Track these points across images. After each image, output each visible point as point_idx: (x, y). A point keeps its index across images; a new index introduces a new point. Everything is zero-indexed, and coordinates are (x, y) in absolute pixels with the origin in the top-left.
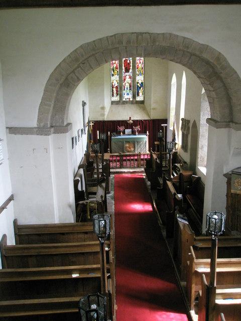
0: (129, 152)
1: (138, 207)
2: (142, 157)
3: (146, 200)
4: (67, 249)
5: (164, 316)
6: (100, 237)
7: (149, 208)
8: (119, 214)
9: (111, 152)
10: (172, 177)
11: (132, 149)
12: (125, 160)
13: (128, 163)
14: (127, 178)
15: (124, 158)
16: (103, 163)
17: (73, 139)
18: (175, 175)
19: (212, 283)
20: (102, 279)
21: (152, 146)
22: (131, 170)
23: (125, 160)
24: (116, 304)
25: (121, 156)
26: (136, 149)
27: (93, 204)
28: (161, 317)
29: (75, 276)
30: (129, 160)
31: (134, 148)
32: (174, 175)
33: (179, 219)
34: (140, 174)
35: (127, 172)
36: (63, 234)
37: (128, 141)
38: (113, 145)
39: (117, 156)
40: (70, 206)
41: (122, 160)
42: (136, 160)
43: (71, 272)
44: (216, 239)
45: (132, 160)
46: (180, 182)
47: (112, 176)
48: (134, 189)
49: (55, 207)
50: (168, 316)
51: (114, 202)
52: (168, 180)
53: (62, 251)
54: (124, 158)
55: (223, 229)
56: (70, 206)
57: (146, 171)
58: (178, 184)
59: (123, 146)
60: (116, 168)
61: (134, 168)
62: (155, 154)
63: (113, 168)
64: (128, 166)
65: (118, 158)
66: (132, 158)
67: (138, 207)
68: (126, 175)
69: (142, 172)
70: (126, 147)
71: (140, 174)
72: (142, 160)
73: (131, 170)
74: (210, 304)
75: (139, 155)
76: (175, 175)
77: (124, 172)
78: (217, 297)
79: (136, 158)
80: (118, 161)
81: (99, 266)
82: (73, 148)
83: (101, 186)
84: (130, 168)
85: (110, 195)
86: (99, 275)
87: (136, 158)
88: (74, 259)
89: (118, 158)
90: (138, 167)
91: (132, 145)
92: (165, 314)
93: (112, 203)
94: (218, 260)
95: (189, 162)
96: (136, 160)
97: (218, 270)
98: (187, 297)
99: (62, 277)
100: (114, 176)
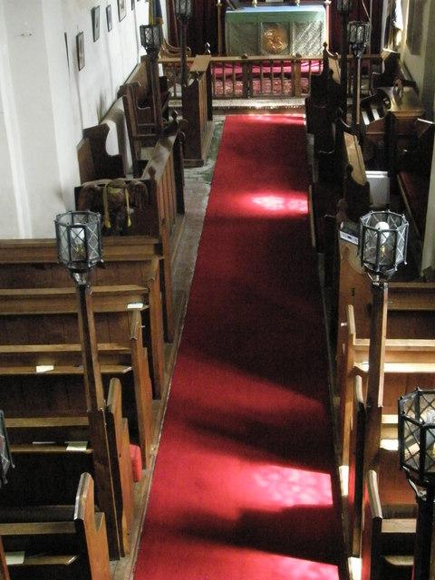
0: (273, 52)
1: (270, 203)
2: (305, 68)
3: (290, 185)
4: (41, 304)
5: (275, 477)
6: (76, 271)
7: (300, 205)
8: (215, 221)
9: (214, 53)
10: (367, 122)
11: (283, 46)
12: (257, 76)
13: (267, 83)
14: (260, 125)
15: (256, 70)
16: (184, 81)
17: (93, 12)
18: (377, 117)
19: (372, 397)
20: (86, 377)
21: (339, 41)
22: (273, 104)
23: (257, 76)
24: (66, 446)
25: (247, 64)
26: (293, 46)
27: (118, 191)
28: (267, 480)
29: (42, 369)
30: (267, 75)
31: (289, 41)
32: (371, 118)
33: (343, 236)
34: (295, 115)
35: (262, 108)
36: (40, 266)
37: (271, 22)
38: (231, 35)
39: (234, 64)
40: (60, 195)
41: (250, 77)
42: (287, 73)
43: (33, 359)
44: (382, 285)
45: (278, 75)
46: (386, 138)
47: (219, 119)
48: (270, 155)
49: (17, 195)
50: (284, 478)
51: (208, 188)
52: (349, 131)
53: (27, 308)
54: (256, 70)
55: (399, 259)
56: (60, 195)
57: (308, 108)
58: (381, 143)
59: (257, 36)
60: (233, 97)
61: (281, 97)
62: (335, 58)
63: (223, 97)
64: (239, 91)
65: (239, 70)
66: (277, 69)
67: (270, 203)
68: (260, 117)
69: (298, 110)
70: (266, 40)
71: (295, 115)
72: (305, 75)
73: (273, 104)
74: (366, 450)
75: (297, 61)
76: (377, 117)
77: (253, 109)
78: (384, 433)
79: (288, 69)
80: (239, 78)
81: (77, 347)
82: (65, 34)
83: (166, 144)
84: (272, 97)
85: (204, 168)
86: (80, 370)
87: (288, 69)
88: (59, 330)
89: (239, 70)
90: (293, 95)
91: (283, 34)
92: (278, 472)
93: (205, 190)
94: (387, 343)
95: (422, 82)
96: (288, 76)
97: (389, 367)
98: (339, 432)
99: (12, 371)
100: (223, 118)
